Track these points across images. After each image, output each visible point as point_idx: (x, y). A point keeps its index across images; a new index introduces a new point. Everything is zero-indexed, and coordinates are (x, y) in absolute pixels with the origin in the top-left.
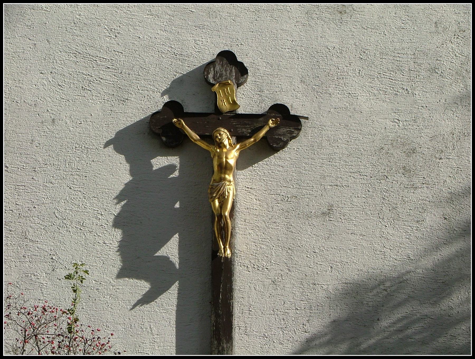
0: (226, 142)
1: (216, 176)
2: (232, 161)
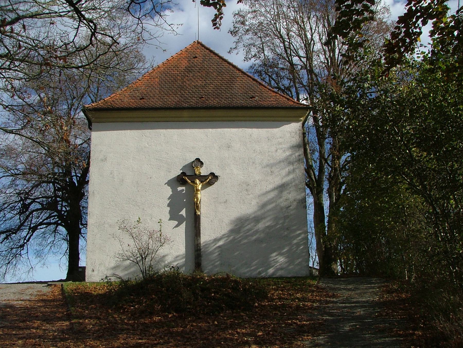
0: (198, 183)
1: (195, 192)
2: (200, 188)
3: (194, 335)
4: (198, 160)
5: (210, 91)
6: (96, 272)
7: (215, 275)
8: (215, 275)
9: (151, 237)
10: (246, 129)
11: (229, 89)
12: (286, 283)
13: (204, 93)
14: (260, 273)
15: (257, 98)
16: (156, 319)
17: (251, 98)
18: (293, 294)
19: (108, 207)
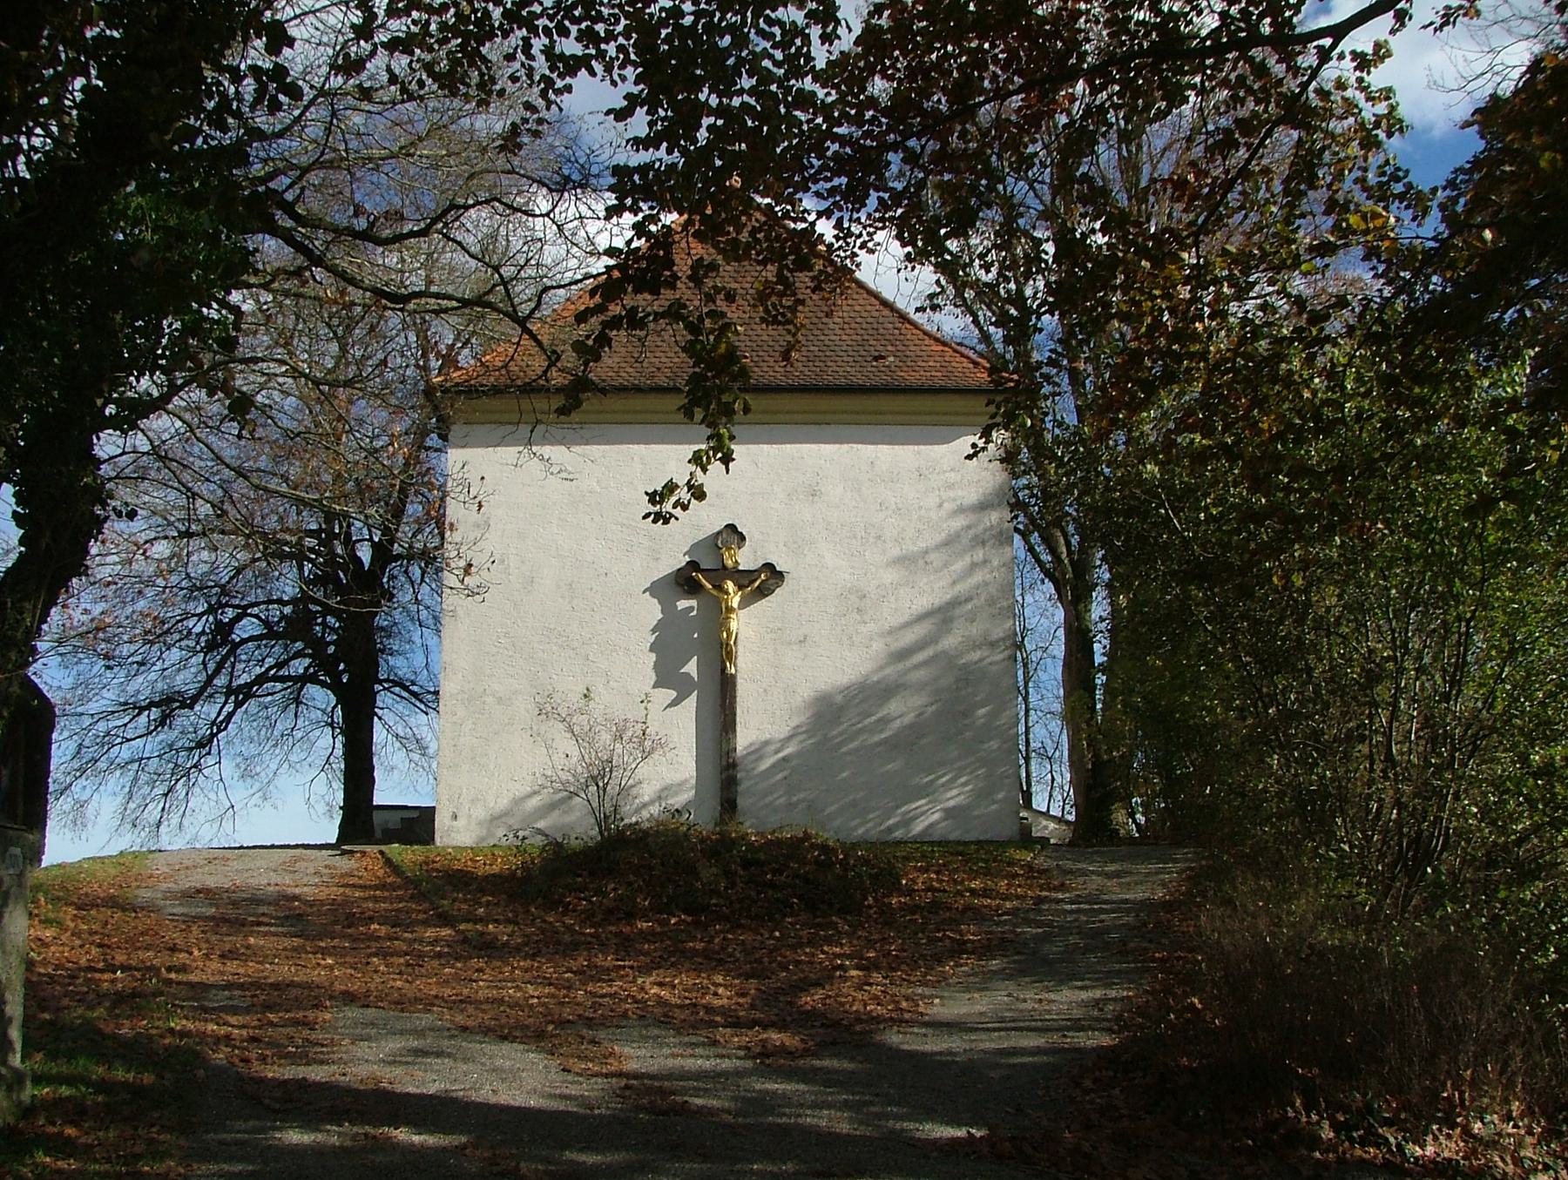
0: (731, 591)
1: (723, 616)
2: (735, 605)
3: (730, 955)
4: (731, 528)
5: (765, 338)
6: (461, 822)
7: (774, 832)
8: (774, 832)
9: (619, 737)
10: (860, 446)
11: (816, 332)
12: (952, 854)
13: (749, 344)
14: (890, 830)
15: (891, 359)
16: (643, 925)
17: (876, 359)
18: (962, 882)
19: (495, 650)
